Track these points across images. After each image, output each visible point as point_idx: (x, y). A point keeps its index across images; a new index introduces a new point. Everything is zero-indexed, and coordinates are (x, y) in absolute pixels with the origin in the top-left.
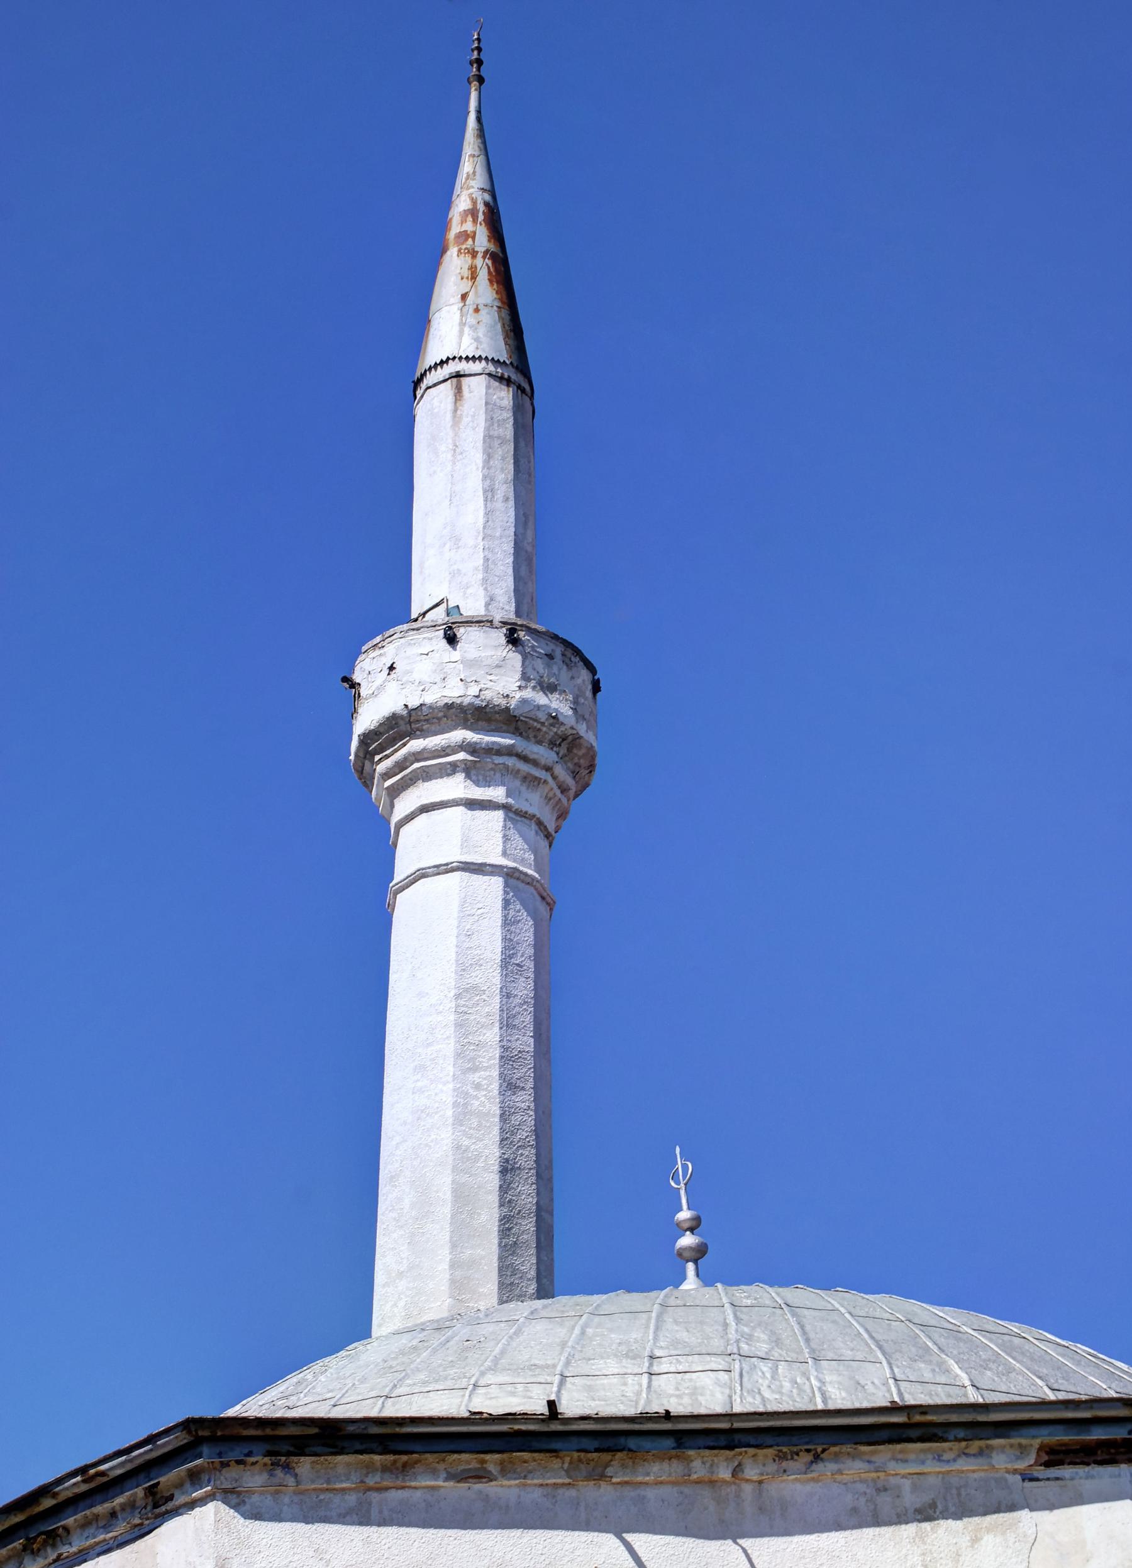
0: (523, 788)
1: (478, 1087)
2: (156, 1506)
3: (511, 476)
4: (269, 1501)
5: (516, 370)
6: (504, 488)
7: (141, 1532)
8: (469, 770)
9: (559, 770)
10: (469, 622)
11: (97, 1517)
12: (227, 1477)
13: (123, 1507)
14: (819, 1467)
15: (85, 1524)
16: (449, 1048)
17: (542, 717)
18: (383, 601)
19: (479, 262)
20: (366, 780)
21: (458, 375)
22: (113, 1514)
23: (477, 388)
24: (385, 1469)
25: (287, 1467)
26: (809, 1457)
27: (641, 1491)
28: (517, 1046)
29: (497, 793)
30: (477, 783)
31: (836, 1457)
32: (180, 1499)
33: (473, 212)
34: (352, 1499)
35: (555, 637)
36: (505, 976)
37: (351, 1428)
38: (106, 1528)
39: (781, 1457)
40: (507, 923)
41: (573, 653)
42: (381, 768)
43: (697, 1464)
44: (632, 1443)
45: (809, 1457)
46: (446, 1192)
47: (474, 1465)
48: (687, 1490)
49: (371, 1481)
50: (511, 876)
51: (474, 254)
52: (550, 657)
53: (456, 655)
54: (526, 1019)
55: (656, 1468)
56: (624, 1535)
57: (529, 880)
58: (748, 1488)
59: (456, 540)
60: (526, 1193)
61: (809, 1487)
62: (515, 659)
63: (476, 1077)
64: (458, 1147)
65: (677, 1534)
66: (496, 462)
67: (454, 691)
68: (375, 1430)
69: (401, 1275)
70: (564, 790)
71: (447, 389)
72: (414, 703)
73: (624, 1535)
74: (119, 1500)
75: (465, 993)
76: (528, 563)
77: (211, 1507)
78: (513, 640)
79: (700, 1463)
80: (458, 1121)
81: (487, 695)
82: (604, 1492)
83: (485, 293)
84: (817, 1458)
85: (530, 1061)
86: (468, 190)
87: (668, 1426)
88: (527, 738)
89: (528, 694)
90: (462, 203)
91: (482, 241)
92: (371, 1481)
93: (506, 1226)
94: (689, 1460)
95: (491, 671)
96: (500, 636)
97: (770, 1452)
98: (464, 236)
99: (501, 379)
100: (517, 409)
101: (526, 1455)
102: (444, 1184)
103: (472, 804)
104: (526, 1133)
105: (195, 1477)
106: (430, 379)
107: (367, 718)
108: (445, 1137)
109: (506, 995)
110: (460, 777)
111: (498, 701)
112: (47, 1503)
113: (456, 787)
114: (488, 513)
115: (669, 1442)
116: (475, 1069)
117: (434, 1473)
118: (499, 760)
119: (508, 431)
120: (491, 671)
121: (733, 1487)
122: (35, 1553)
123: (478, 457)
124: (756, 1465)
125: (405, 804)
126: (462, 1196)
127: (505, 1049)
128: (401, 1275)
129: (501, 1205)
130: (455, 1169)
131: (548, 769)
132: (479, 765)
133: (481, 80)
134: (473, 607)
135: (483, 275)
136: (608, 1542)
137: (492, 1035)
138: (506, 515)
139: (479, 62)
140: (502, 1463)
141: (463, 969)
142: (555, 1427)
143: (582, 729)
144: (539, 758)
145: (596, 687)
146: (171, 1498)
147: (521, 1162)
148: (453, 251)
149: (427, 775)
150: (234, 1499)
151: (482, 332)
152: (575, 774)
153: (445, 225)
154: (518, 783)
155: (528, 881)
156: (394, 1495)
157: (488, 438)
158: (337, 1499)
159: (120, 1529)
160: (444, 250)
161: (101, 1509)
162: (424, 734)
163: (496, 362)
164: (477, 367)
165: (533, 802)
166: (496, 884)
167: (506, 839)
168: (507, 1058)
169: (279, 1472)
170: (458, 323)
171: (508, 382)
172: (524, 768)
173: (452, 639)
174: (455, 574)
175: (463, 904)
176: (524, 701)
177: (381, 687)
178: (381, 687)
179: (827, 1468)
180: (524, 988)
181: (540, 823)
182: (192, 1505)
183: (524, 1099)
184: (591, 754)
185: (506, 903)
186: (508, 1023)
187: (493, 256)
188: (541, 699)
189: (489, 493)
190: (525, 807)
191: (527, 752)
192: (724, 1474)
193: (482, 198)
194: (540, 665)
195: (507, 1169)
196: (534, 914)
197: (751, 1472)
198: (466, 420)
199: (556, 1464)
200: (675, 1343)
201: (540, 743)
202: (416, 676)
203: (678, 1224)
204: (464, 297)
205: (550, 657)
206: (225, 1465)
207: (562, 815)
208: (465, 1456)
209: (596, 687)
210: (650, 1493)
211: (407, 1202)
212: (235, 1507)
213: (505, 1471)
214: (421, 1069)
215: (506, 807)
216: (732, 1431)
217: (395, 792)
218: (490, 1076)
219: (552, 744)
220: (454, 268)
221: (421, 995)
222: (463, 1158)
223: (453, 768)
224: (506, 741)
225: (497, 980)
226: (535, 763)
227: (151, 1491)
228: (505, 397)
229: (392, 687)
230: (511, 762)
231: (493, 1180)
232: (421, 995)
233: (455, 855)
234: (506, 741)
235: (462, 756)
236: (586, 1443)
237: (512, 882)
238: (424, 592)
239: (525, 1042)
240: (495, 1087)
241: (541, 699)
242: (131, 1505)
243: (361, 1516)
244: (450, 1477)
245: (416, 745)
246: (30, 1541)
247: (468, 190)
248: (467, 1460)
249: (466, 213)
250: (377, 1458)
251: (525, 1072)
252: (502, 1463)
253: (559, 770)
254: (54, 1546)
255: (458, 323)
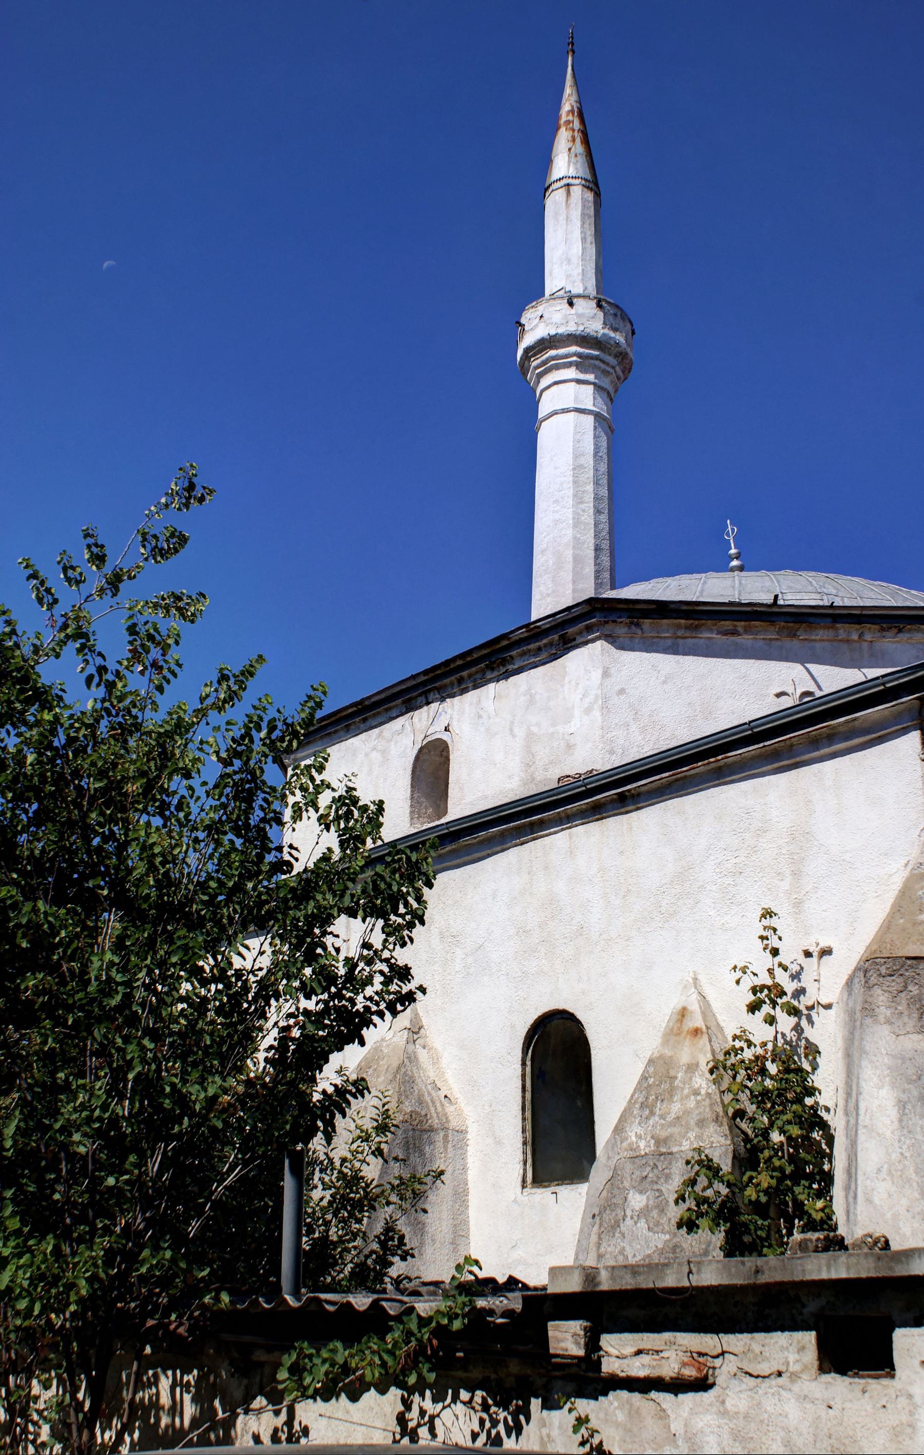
1: (584, 511)
2: (565, 644)
4: (627, 641)
5: (593, 184)
6: (590, 238)
7: (555, 657)
8: (578, 366)
9: (618, 368)
10: (579, 296)
11: (529, 651)
12: (608, 629)
13: (545, 645)
14: (901, 635)
15: (523, 654)
16: (570, 492)
17: (612, 342)
18: (534, 290)
19: (576, 134)
20: (524, 368)
21: (568, 185)
22: (539, 649)
23: (577, 191)
24: (687, 628)
25: (638, 625)
26: (896, 631)
27: (813, 644)
28: (601, 494)
29: (591, 377)
31: (910, 631)
32: (577, 642)
33: (572, 111)
34: (669, 642)
35: (617, 306)
36: (595, 461)
37: (672, 606)
38: (535, 656)
39: (883, 629)
40: (595, 437)
41: (624, 317)
42: (534, 364)
43: (841, 631)
44: (811, 619)
45: (896, 631)
46: (570, 558)
47: (731, 627)
48: (835, 644)
49: (680, 633)
50: (597, 416)
51: (573, 130)
52: (615, 315)
53: (573, 311)
54: (605, 481)
55: (821, 632)
58: (865, 645)
59: (569, 261)
60: (606, 560)
61: (894, 646)
62: (601, 315)
63: (583, 506)
64: (575, 538)
65: (831, 665)
66: (586, 226)
67: (571, 328)
68: (684, 607)
69: (548, 595)
70: (619, 379)
71: (562, 192)
72: (553, 332)
74: (545, 641)
75: (577, 468)
76: (601, 272)
77: (599, 643)
78: (599, 305)
79: (843, 630)
80: (575, 525)
81: (587, 330)
82: (795, 644)
83: (579, 148)
84: (900, 631)
85: (606, 501)
86: (568, 102)
87: (830, 611)
89: (606, 331)
90: (566, 107)
91: (577, 124)
92: (680, 633)
94: (837, 629)
95: (589, 319)
96: (593, 304)
97: (877, 627)
98: (568, 122)
99: (588, 188)
100: (595, 203)
101: (757, 623)
102: (569, 554)
103: (579, 382)
104: (605, 533)
105: (589, 629)
106: (554, 186)
107: (528, 340)
108: (569, 533)
109: (596, 470)
110: (574, 368)
112: (505, 643)
113: (571, 373)
114: (584, 249)
115: (829, 620)
116: (582, 503)
117: (711, 631)
118: (592, 362)
119: (592, 212)
120: (589, 319)
121: (857, 645)
122: (493, 669)
123: (578, 223)
124: (870, 633)
125: (545, 381)
126: (577, 560)
127: (596, 494)
128: (548, 595)
130: (574, 548)
131: (613, 368)
132: (583, 364)
133: (573, 52)
134: (578, 289)
135: (578, 141)
136: (798, 667)
137: (590, 488)
138: (592, 250)
139: (573, 44)
140: (745, 627)
141: (576, 457)
142: (775, 610)
143: (629, 350)
144: (607, 361)
145: (633, 333)
146: (574, 640)
147: (603, 546)
148: (563, 129)
149: (557, 367)
150: (611, 640)
151: (579, 165)
152: (623, 372)
153: (558, 118)
155: (604, 419)
156: (690, 641)
157: (583, 215)
158: (662, 642)
159: (543, 656)
160: (558, 128)
161: (532, 646)
162: (557, 348)
163: (586, 180)
164: (577, 181)
165: (606, 383)
166: (590, 419)
167: (594, 398)
168: (597, 498)
169: (633, 627)
170: (565, 162)
171: (591, 190)
172: (603, 366)
173: (571, 304)
174: (568, 276)
175: (575, 427)
176: (604, 335)
177: (537, 325)
178: (537, 325)
179: (903, 636)
180: (603, 467)
181: (608, 393)
182: (586, 643)
183: (604, 518)
184: (631, 363)
185: (595, 428)
186: (597, 483)
187: (583, 132)
188: (612, 334)
189: (584, 240)
190: (603, 385)
192: (855, 637)
193: (576, 105)
194: (611, 318)
195: (597, 549)
196: (606, 434)
197: (868, 637)
198: (572, 206)
199: (772, 628)
200: (790, 587)
202: (554, 320)
203: (730, 556)
204: (570, 150)
205: (615, 315)
206: (606, 622)
207: (616, 391)
208: (727, 623)
209: (633, 333)
210: (818, 645)
211: (551, 562)
212: (612, 643)
213: (747, 630)
214: (556, 501)
215: (594, 384)
216: (861, 615)
217: (540, 376)
218: (589, 506)
219: (616, 356)
220: (563, 139)
221: (556, 468)
222: (577, 543)
223: (570, 365)
224: (597, 353)
225: (592, 463)
226: (608, 364)
227: (562, 637)
228: (590, 196)
229: (542, 325)
230: (597, 363)
231: (591, 554)
232: (556, 468)
233: (572, 405)
234: (597, 353)
235: (575, 358)
236: (788, 618)
238: (551, 285)
239: (604, 492)
240: (592, 511)
241: (612, 334)
242: (551, 644)
243: (674, 650)
244: (719, 633)
245: (553, 353)
246: (492, 663)
247: (568, 102)
248: (727, 624)
249: (568, 112)
250: (683, 621)
251: (605, 505)
252: (745, 627)
253: (618, 368)
254: (504, 665)
255: (565, 162)
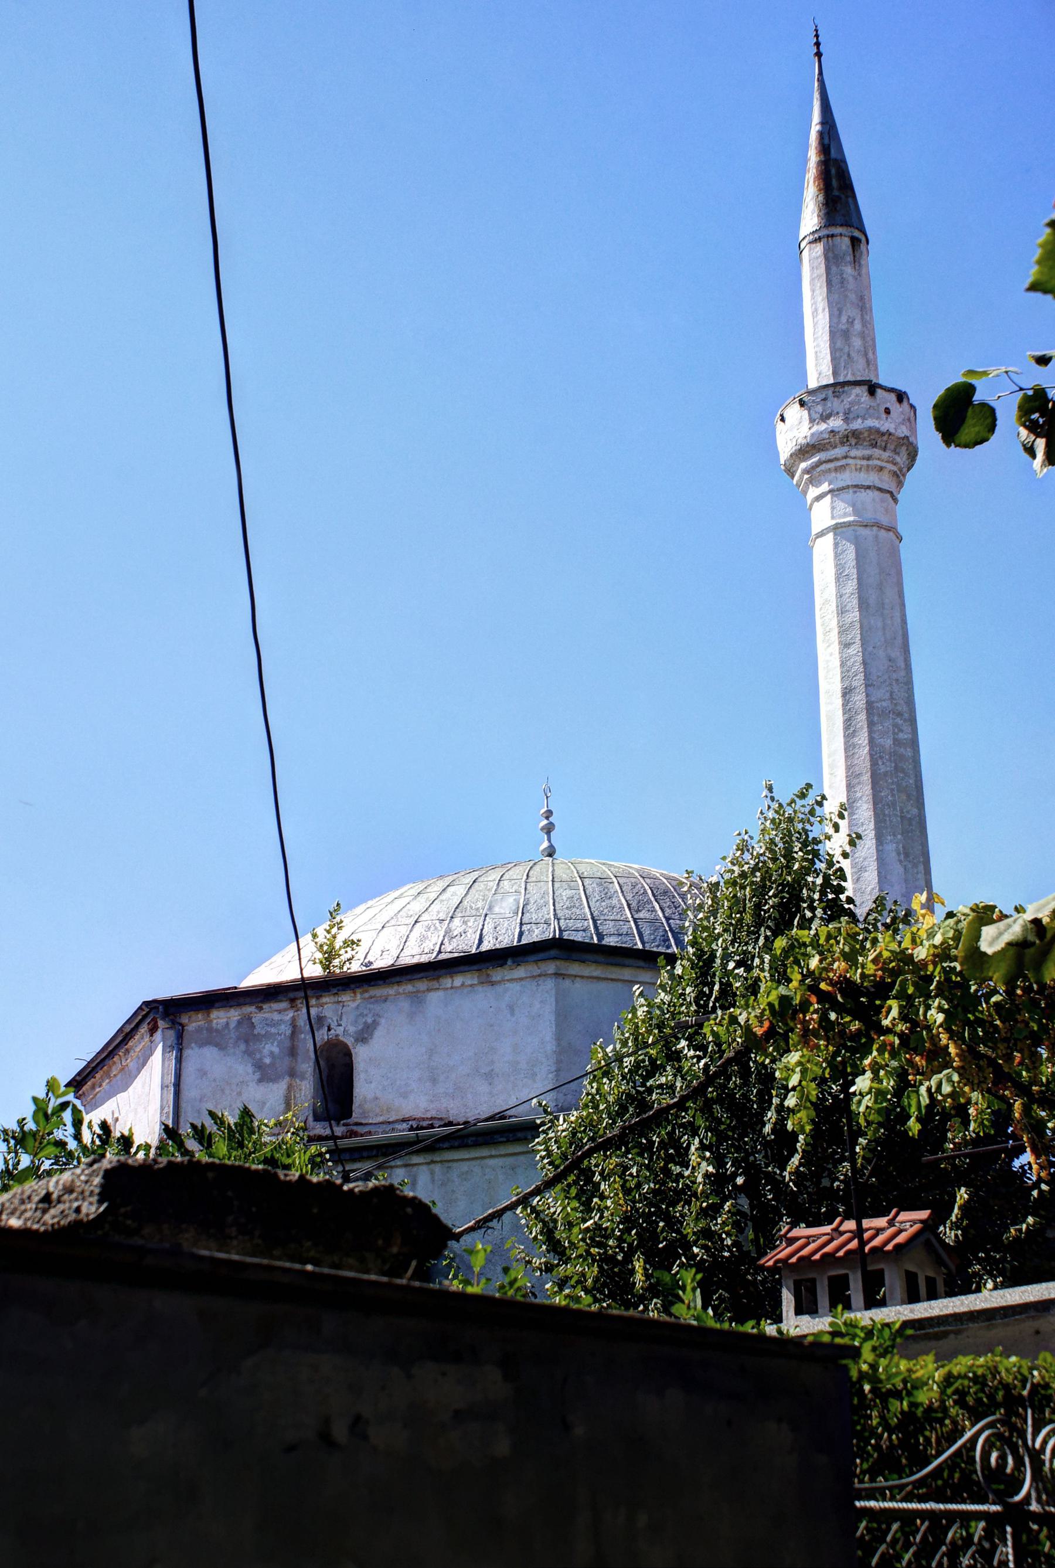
0: (838, 475)
3: (825, 295)
29: (825, 487)
30: (817, 487)
56: (854, 1379)
57: (470, 1141)
73: (854, 1379)
88: (827, 450)
93: (848, 723)
111: (804, 441)
118: (818, 469)
129: (844, 714)
131: (846, 457)
132: (814, 476)
154: (833, 474)
172: (831, 465)
176: (812, 435)
191: (829, 457)
201: (835, 447)
215: (830, 491)
219: (842, 444)
230: (823, 467)
237: (838, 531)
241: (823, 426)
